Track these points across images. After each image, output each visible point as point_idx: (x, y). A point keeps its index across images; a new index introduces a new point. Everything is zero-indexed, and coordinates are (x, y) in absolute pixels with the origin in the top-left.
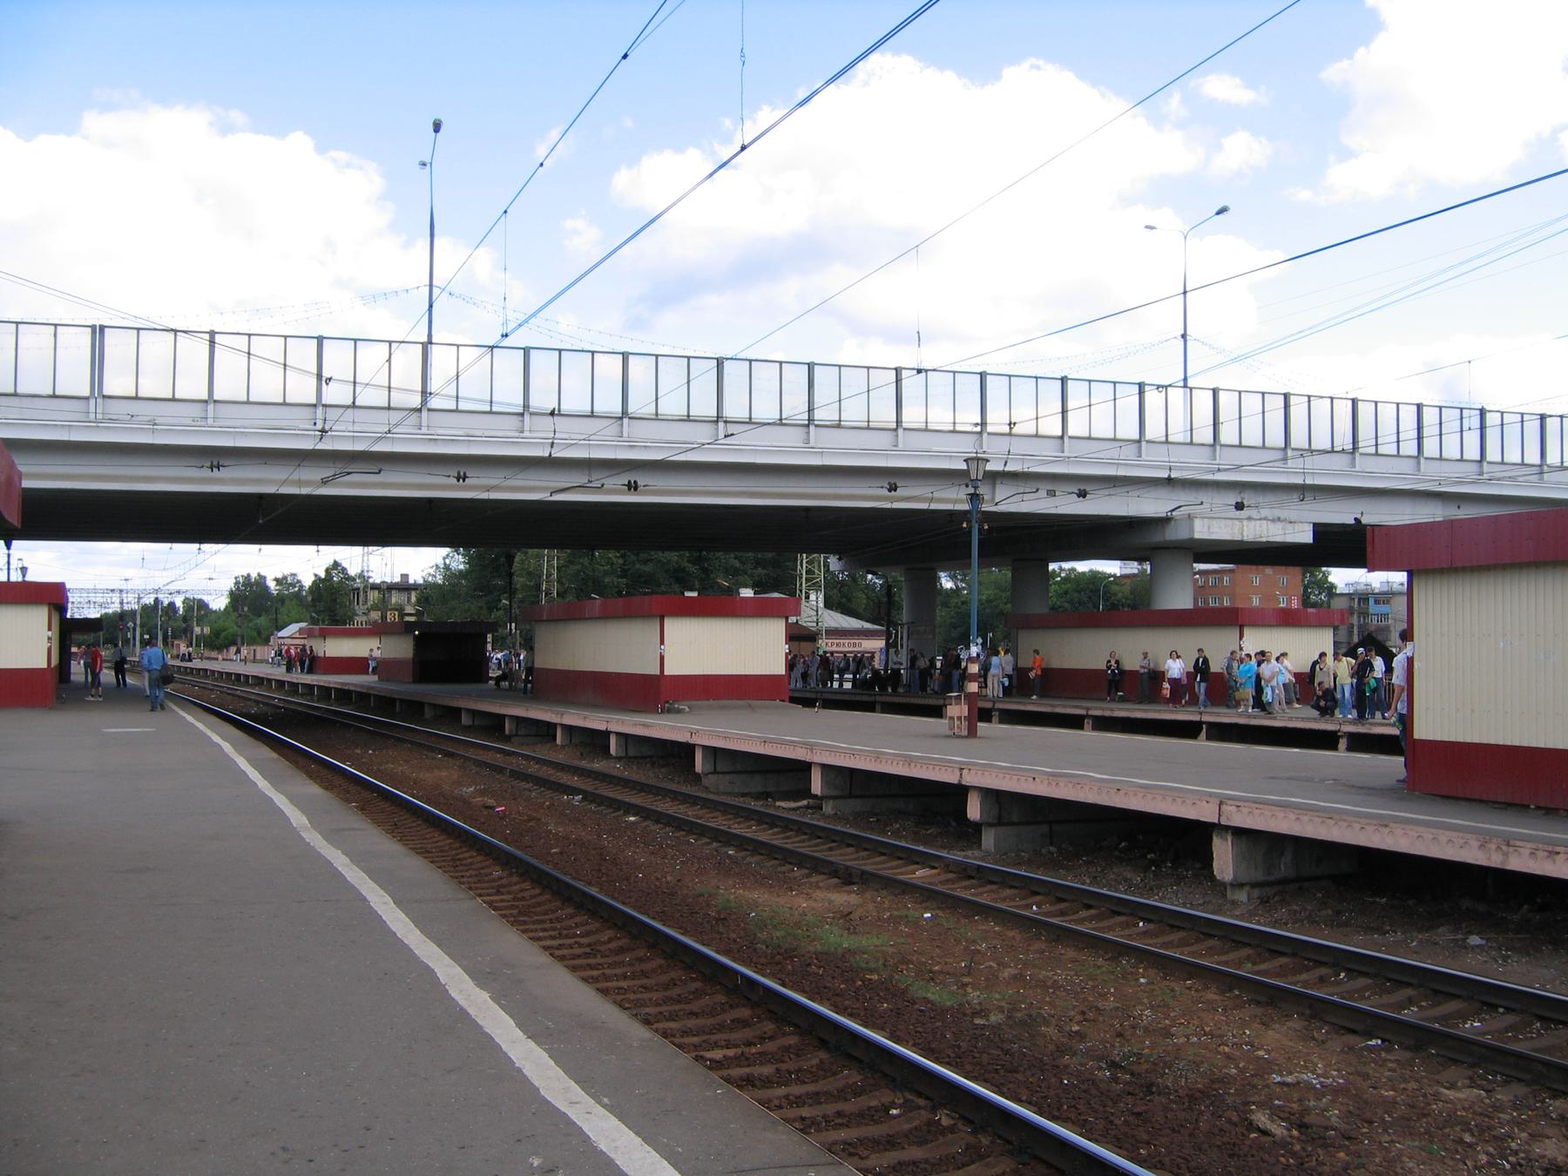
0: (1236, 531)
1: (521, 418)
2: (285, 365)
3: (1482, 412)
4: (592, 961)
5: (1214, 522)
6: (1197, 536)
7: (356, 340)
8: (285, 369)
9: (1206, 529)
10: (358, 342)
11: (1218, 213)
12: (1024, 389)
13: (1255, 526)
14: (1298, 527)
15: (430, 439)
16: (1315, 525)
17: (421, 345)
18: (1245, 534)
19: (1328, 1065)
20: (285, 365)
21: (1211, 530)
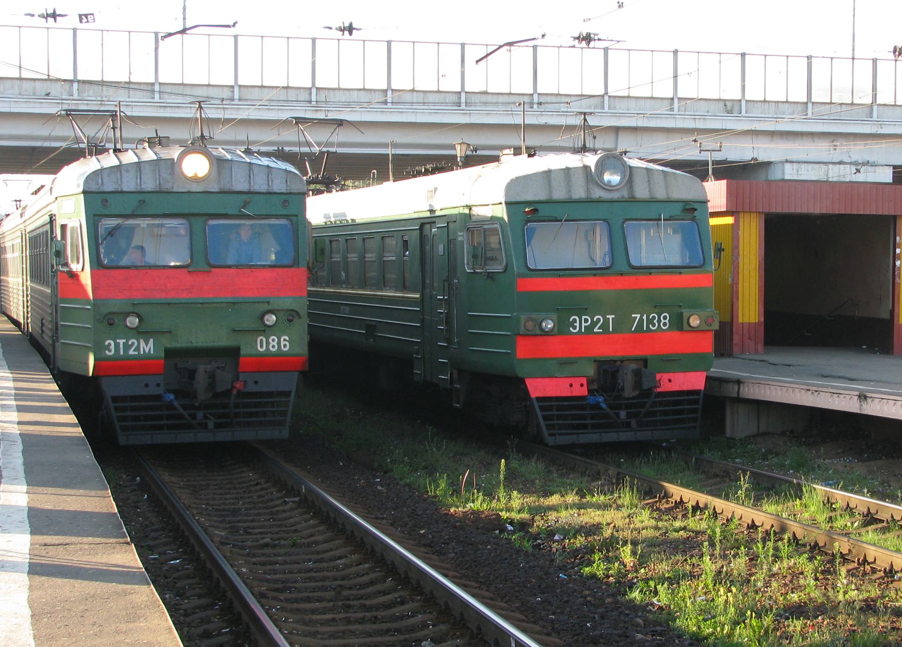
0: (822, 173)
1: (232, 90)
2: (20, 67)
3: (88, 22)
4: (368, 515)
5: (803, 166)
6: (787, 177)
7: (414, 42)
8: (20, 69)
9: (795, 171)
10: (131, 33)
11: (46, 16)
12: (776, 65)
13: (839, 169)
14: (880, 170)
15: (161, 106)
16: (895, 167)
17: (386, 43)
18: (830, 176)
19: (717, 452)
20: (20, 67)
21: (799, 172)
